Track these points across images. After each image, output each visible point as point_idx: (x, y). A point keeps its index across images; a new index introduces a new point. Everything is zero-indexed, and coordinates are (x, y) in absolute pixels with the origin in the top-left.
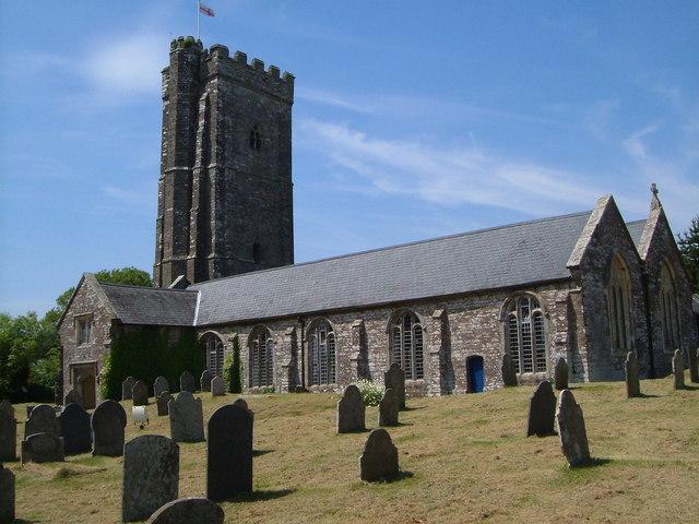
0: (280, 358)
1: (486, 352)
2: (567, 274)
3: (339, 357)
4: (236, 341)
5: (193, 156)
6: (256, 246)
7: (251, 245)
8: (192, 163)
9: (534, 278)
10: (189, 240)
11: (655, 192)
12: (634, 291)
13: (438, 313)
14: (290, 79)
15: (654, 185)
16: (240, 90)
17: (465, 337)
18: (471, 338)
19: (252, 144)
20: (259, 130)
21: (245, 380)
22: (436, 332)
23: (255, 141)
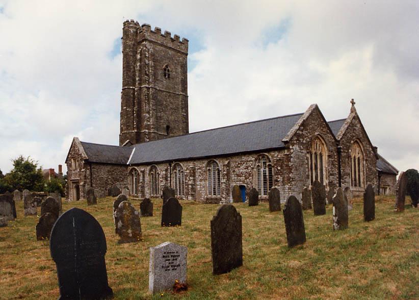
0: (162, 181)
1: (247, 184)
2: (283, 145)
3: (186, 182)
4: (143, 172)
5: (134, 80)
6: (168, 127)
7: (165, 126)
8: (134, 85)
9: (268, 147)
10: (134, 123)
11: (353, 103)
12: (329, 156)
13: (226, 162)
14: (186, 41)
15: (353, 100)
16: (158, 48)
17: (238, 176)
18: (240, 176)
19: (165, 76)
20: (169, 68)
21: (217, 193)
22: (225, 173)
23: (166, 74)
